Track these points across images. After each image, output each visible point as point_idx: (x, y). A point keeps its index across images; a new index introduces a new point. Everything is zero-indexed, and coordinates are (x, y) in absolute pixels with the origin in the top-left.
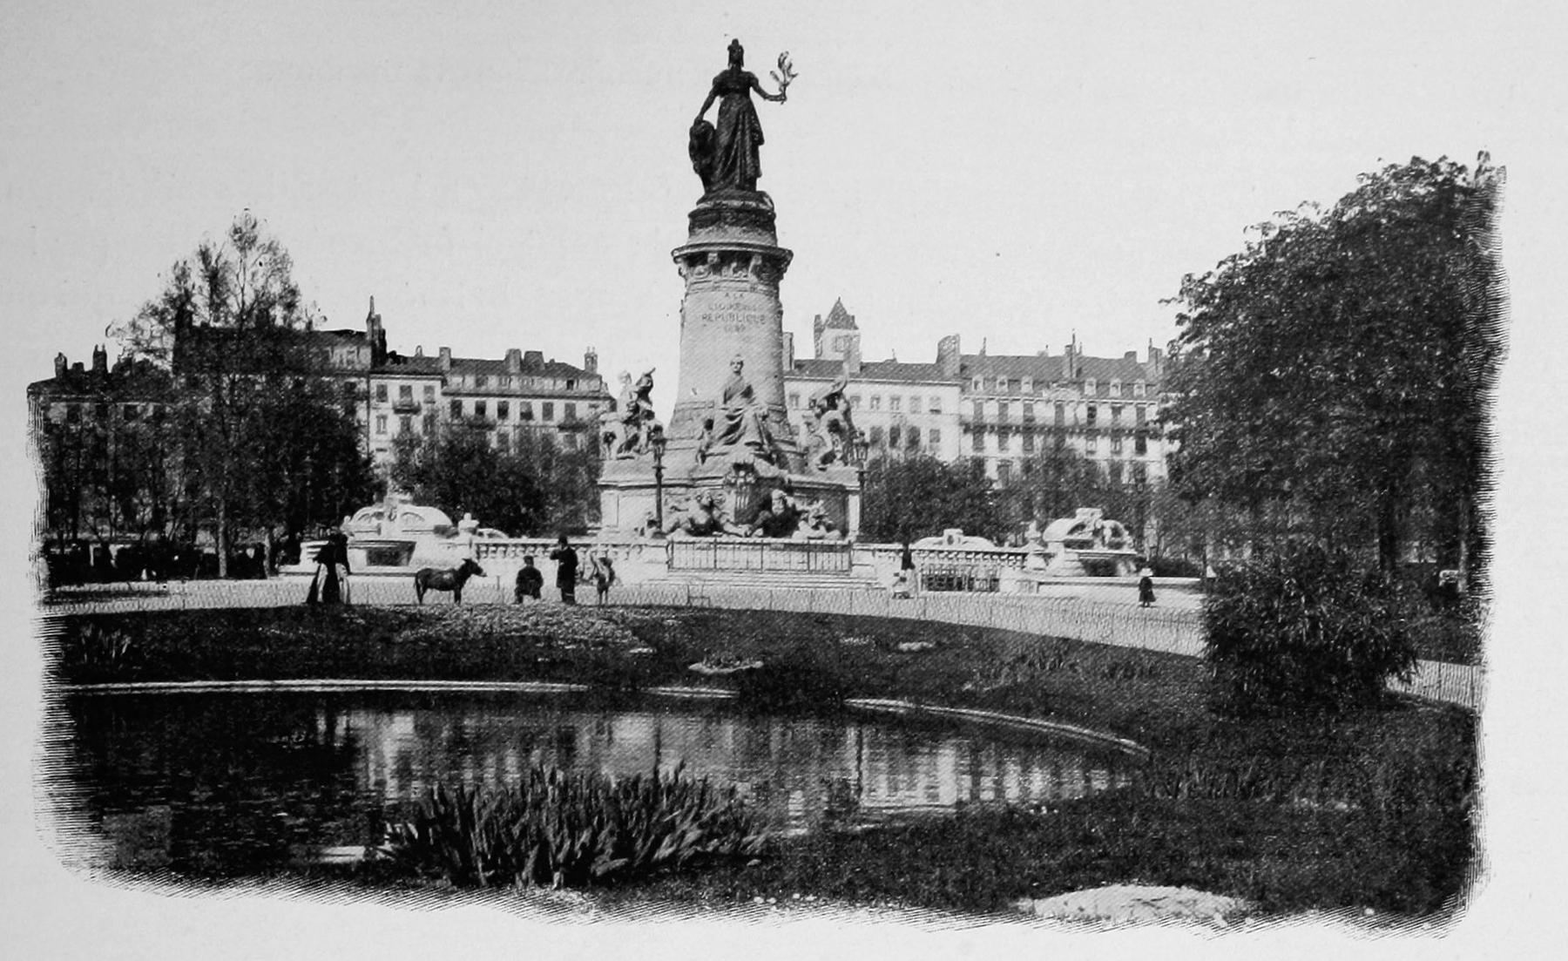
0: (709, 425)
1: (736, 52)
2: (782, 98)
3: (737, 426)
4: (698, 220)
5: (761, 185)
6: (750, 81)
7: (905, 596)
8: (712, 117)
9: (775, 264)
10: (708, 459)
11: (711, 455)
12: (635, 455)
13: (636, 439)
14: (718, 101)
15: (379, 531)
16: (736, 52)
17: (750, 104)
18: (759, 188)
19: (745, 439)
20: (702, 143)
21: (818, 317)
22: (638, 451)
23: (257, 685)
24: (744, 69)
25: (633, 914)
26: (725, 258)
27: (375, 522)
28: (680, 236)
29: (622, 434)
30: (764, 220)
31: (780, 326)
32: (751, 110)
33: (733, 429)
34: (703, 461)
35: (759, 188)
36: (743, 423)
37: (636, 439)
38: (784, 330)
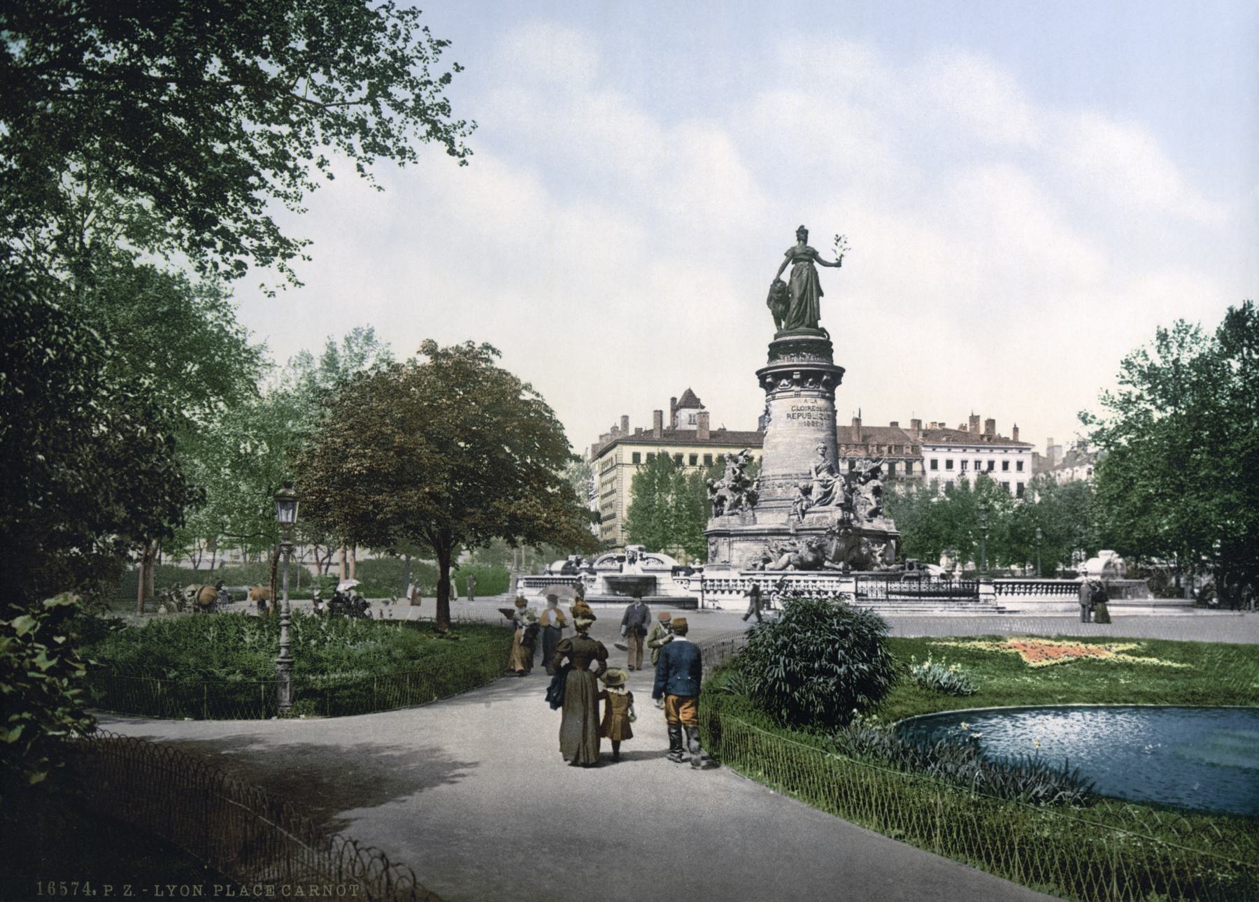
0: (807, 491)
1: (802, 234)
2: (838, 265)
3: (831, 491)
4: (776, 350)
5: (821, 324)
6: (813, 255)
7: (107, 605)
8: (786, 277)
9: (837, 375)
10: (807, 516)
11: (810, 513)
12: (740, 512)
13: (739, 500)
14: (790, 266)
15: (621, 570)
16: (802, 234)
17: (815, 269)
18: (820, 326)
19: (835, 502)
20: (779, 298)
21: (674, 399)
22: (742, 509)
23: (1167, 663)
24: (808, 244)
25: (1175, 801)
26: (805, 375)
27: (617, 564)
28: (763, 362)
29: (730, 497)
30: (824, 348)
31: (835, 421)
32: (815, 273)
33: (827, 494)
34: (803, 517)
35: (820, 326)
36: (834, 491)
37: (739, 500)
38: (839, 424)
